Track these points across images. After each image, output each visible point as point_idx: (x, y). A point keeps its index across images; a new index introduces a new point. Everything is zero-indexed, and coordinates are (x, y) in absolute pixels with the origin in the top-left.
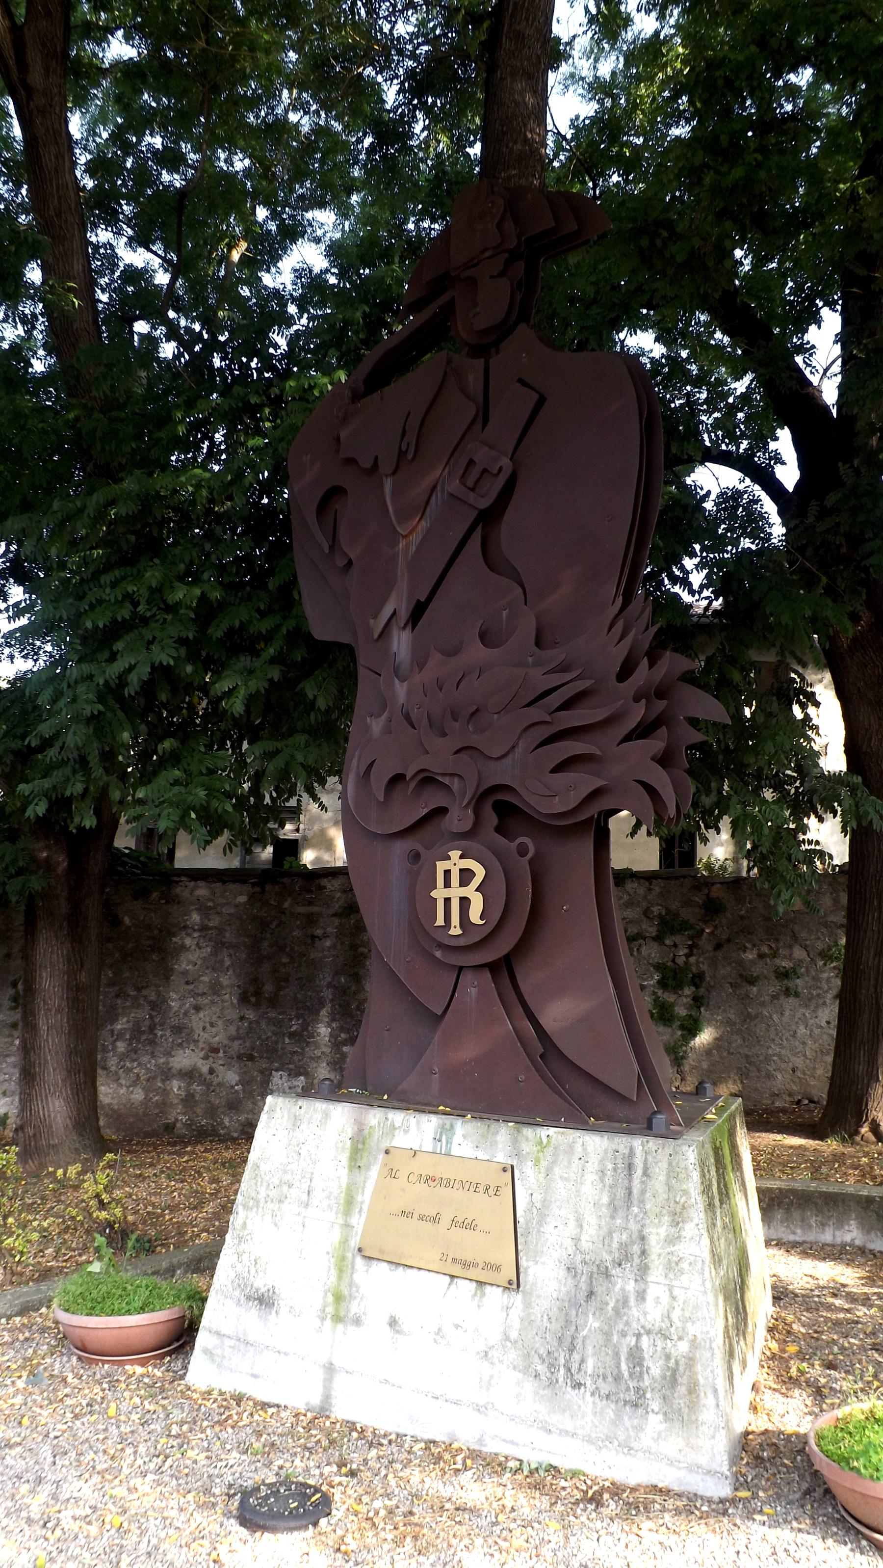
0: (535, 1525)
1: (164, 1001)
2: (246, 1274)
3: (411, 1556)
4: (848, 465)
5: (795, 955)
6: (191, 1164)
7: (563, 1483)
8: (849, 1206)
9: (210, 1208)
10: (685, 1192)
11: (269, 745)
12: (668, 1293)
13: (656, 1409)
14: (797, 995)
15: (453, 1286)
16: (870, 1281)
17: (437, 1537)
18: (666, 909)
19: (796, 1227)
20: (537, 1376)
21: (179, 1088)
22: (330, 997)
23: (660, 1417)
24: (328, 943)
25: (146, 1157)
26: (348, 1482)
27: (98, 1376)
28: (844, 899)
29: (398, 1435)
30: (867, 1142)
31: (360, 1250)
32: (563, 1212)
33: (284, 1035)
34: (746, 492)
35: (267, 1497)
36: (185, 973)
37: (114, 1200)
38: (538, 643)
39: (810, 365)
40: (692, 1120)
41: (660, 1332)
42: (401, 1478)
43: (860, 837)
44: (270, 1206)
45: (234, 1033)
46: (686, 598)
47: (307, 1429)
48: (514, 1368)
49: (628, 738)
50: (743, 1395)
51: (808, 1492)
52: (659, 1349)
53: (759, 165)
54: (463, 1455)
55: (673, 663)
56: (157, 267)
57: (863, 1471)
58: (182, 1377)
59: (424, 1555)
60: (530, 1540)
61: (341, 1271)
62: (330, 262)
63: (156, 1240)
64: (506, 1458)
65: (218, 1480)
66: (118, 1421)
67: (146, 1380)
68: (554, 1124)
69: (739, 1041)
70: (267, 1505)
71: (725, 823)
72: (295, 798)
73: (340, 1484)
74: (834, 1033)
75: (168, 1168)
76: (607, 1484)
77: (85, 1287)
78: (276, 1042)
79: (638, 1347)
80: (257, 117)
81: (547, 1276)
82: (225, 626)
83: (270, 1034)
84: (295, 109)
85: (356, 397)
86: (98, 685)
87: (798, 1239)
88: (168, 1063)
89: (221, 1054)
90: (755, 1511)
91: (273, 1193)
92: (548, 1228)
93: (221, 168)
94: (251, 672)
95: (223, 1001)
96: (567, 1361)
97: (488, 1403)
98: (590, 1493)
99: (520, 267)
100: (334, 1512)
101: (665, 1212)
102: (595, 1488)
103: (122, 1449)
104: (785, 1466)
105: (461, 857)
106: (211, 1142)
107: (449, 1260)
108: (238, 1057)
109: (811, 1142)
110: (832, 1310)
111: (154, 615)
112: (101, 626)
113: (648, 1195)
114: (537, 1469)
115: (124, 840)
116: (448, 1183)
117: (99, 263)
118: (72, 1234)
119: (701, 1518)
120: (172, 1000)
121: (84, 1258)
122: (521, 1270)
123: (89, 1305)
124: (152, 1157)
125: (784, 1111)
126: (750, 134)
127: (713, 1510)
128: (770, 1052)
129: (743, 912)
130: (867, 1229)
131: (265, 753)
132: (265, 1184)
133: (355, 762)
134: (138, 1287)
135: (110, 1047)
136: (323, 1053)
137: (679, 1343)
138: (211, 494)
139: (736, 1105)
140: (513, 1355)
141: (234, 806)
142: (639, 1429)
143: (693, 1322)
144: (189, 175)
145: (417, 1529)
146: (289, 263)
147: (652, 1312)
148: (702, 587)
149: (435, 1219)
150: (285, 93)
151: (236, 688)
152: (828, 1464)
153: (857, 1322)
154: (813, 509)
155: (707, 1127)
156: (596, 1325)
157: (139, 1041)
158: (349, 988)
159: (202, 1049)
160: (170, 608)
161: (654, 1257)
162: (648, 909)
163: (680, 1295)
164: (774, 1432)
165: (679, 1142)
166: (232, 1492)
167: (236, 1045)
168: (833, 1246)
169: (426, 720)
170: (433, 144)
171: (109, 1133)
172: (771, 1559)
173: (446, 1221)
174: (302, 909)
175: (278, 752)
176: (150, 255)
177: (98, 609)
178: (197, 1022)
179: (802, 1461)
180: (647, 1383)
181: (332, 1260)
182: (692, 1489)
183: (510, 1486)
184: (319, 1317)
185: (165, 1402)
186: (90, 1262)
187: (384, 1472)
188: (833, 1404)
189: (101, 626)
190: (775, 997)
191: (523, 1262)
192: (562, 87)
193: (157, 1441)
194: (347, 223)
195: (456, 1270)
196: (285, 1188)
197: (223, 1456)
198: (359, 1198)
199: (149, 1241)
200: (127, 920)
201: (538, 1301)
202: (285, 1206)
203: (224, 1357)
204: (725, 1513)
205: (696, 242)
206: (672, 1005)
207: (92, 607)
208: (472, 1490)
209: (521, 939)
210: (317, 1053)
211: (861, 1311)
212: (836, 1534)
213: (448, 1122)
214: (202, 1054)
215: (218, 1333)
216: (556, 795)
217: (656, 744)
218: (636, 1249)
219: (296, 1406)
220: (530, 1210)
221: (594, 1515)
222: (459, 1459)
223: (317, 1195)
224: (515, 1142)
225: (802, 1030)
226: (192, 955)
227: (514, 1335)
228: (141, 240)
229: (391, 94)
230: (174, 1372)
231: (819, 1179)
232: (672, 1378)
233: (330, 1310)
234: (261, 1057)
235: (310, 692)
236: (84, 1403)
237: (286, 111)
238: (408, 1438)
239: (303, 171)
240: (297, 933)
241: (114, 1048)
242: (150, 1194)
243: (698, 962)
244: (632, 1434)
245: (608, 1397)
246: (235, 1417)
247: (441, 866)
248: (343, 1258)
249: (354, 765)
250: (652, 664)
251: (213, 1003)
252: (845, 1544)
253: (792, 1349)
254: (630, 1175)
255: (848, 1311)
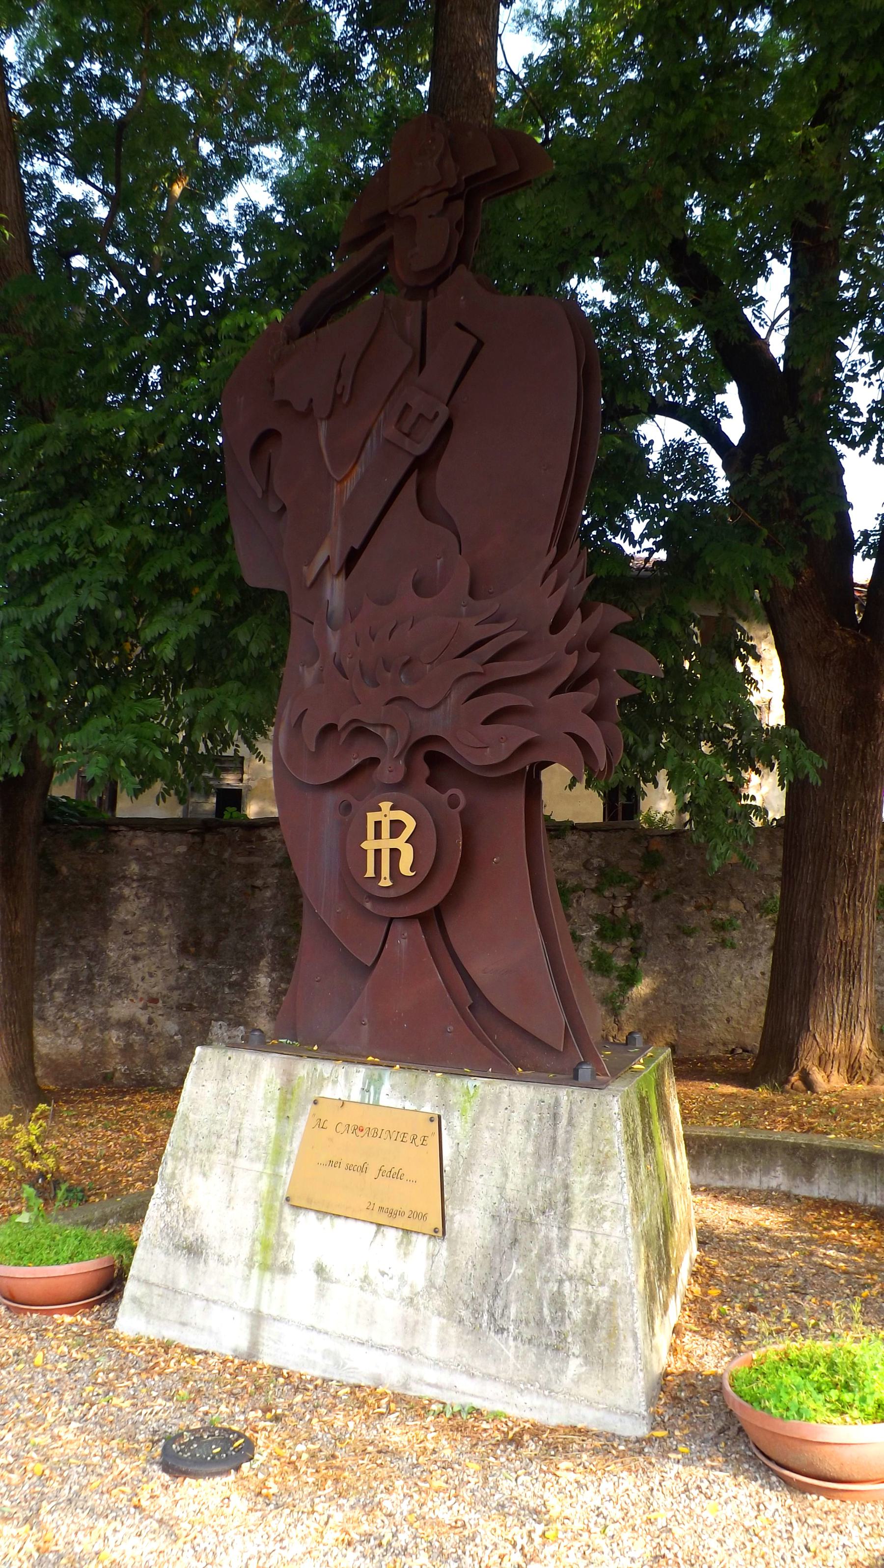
0: (456, 1466)
1: (103, 951)
2: (174, 1224)
3: (331, 1499)
4: (792, 420)
5: (731, 907)
6: (128, 1113)
7: (485, 1425)
8: (776, 1153)
9: (145, 1157)
10: (609, 1142)
11: (199, 692)
12: (590, 1240)
13: (577, 1353)
14: (733, 946)
15: (380, 1235)
16: (794, 1225)
17: (358, 1480)
18: (606, 861)
19: (724, 1172)
20: (461, 1321)
21: (118, 1038)
22: (270, 947)
23: (580, 1361)
24: (268, 894)
25: (83, 1107)
26: (272, 1427)
27: (26, 1326)
28: (780, 853)
29: (324, 1380)
30: (796, 1090)
31: (288, 1199)
32: (488, 1162)
33: (224, 985)
34: (692, 445)
35: (190, 1442)
36: (124, 923)
37: (46, 1150)
38: (472, 594)
39: (759, 318)
40: (619, 1070)
41: (582, 1277)
42: (325, 1423)
43: (796, 792)
44: (199, 1156)
45: (173, 983)
46: (628, 549)
47: (234, 1375)
48: (439, 1314)
49: (559, 690)
50: (664, 1337)
51: (722, 1431)
52: (580, 1294)
53: (710, 109)
54: (387, 1399)
55: (608, 615)
56: (96, 199)
57: (773, 1411)
58: (111, 1326)
59: (345, 1497)
60: (450, 1481)
61: (269, 1220)
62: (276, 199)
63: (89, 1190)
64: (430, 1401)
65: (142, 1427)
66: (45, 1370)
67: (75, 1329)
68: (484, 1074)
69: (676, 992)
70: (189, 1450)
71: (662, 776)
72: (233, 748)
73: (264, 1429)
74: (767, 983)
75: (105, 1118)
76: (528, 1425)
77: (14, 1237)
78: (216, 992)
79: (560, 1293)
80: (200, 45)
81: (472, 1223)
82: (155, 571)
83: (209, 984)
84: (241, 39)
85: (291, 338)
86: (25, 629)
87: (725, 1185)
88: (106, 1013)
89: (160, 1004)
90: (670, 1450)
91: (202, 1143)
92: (474, 1178)
93: (164, 98)
94: (182, 617)
95: (162, 951)
96: (490, 1307)
97: (413, 1348)
98: (511, 1435)
99: (459, 207)
100: (257, 1456)
101: (588, 1160)
102: (516, 1429)
103: (48, 1398)
104: (702, 1405)
105: (392, 808)
106: (150, 1091)
107: (376, 1208)
108: (177, 1007)
109: (742, 1090)
110: (755, 1254)
111: (83, 558)
112: (28, 568)
113: (572, 1144)
114: (459, 1412)
115: (63, 789)
116: (375, 1133)
117: (35, 194)
118: (5, 1184)
119: (617, 1457)
120: (111, 950)
121: (16, 1208)
122: (447, 1218)
123: (17, 1255)
124: (90, 1107)
125: (718, 1059)
126: (702, 78)
127: (630, 1449)
128: (706, 1002)
129: (681, 865)
130: (793, 1176)
131: (196, 700)
132: (194, 1135)
133: (286, 712)
134: (67, 1236)
135: (48, 998)
136: (263, 1003)
137: (600, 1289)
138: (142, 434)
139: (665, 1055)
140: (438, 1302)
141: (165, 755)
142: (560, 1372)
143: (614, 1268)
144: (130, 104)
145: (338, 1472)
146: (231, 201)
147: (575, 1258)
148: (643, 536)
149: (363, 1169)
150: (231, 22)
151: (167, 633)
152: (741, 1404)
153: (778, 1266)
154: (757, 463)
155: (634, 1077)
156: (520, 1271)
157: (77, 992)
158: (290, 938)
159: (141, 999)
160: (101, 552)
161: (577, 1204)
162: (588, 861)
163: (604, 1242)
164: (692, 1373)
165: (604, 1092)
166: (157, 1438)
167: (176, 995)
168: (760, 1191)
169: (358, 668)
170: (381, 79)
171: (48, 1084)
172: (683, 1496)
173: (373, 1171)
174: (241, 860)
175: (210, 699)
176: (89, 188)
177: (25, 552)
178: (136, 971)
179: (718, 1400)
180: (568, 1327)
181: (260, 1209)
182: (610, 1429)
183: (432, 1429)
184: (246, 1265)
185: (93, 1350)
186: (20, 1213)
187: (308, 1417)
188: (750, 1345)
189: (28, 568)
190: (711, 949)
191: (449, 1211)
192: (515, 24)
193: (83, 1389)
194: (294, 159)
195: (383, 1219)
196: (214, 1139)
197: (148, 1404)
198: (288, 1149)
199: (82, 1191)
200: (64, 870)
201: (463, 1249)
202: (214, 1157)
203: (152, 1305)
204: (641, 1452)
205: (646, 188)
206: (611, 956)
207: (19, 550)
208: (396, 1433)
209: (451, 891)
210: (257, 1003)
211: (784, 1255)
212: (747, 1470)
213: (376, 1073)
214: (140, 1004)
215: (147, 1282)
216: (488, 747)
217: (588, 696)
218: (560, 1197)
219: (224, 1352)
220: (456, 1160)
221: (513, 1455)
222: (384, 1402)
223: (246, 1144)
224: (442, 1092)
225: (737, 981)
226: (131, 906)
227: (439, 1281)
228: (79, 171)
229: (339, 25)
230: (103, 1320)
231: (748, 1127)
232: (593, 1323)
233: (258, 1258)
234: (201, 1008)
235: (243, 638)
236: (11, 1352)
237: (232, 40)
238: (334, 1383)
239: (251, 104)
240: (236, 884)
241: (52, 998)
242: (86, 1144)
243: (636, 913)
244: (553, 1377)
245: (530, 1341)
246: (163, 1365)
247: (372, 817)
248: (271, 1208)
249: (287, 712)
250: (584, 617)
251: (152, 953)
252: (756, 1480)
253: (714, 1292)
254: (555, 1125)
255: (771, 1254)
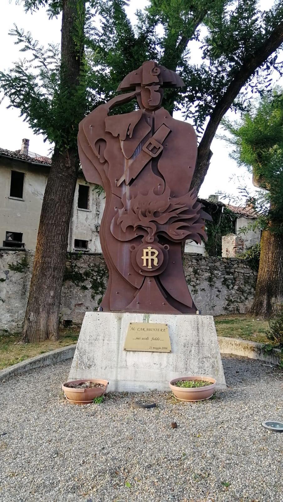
105: (151, 248)
107: (152, 348)
149: (147, 339)
173: (150, 339)
247: (145, 251)
